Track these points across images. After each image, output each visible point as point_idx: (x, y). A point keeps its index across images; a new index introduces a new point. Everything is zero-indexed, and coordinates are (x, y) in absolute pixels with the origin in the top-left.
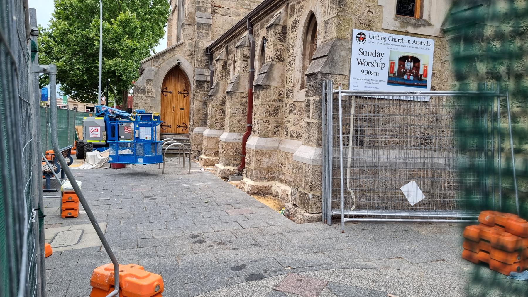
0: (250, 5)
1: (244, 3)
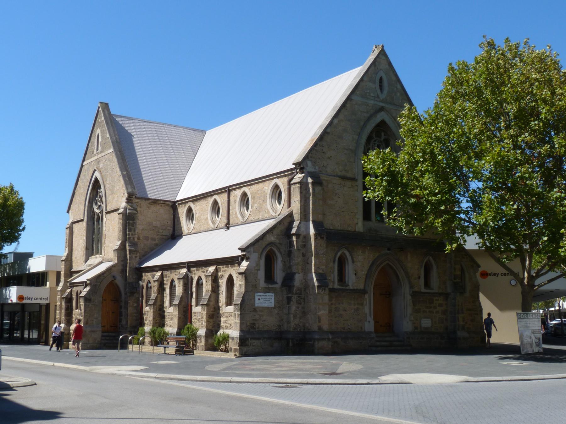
0: (163, 233)
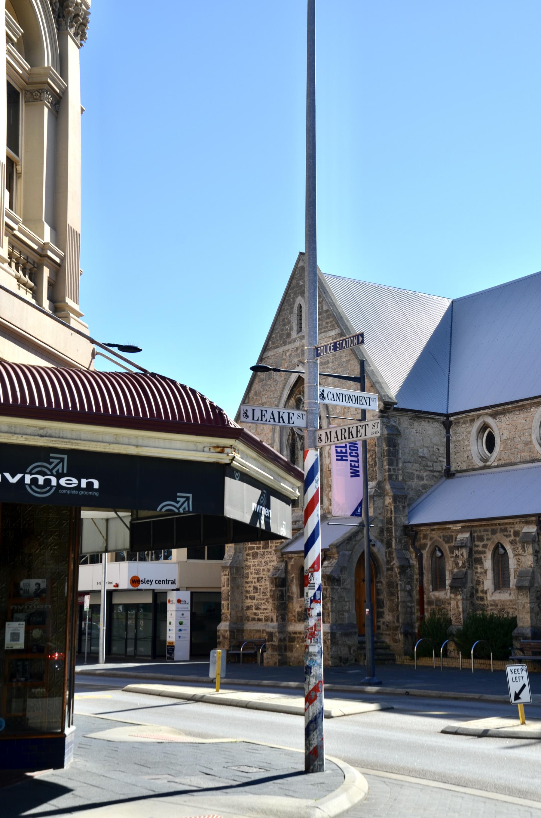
0: (433, 466)
1: (427, 464)
